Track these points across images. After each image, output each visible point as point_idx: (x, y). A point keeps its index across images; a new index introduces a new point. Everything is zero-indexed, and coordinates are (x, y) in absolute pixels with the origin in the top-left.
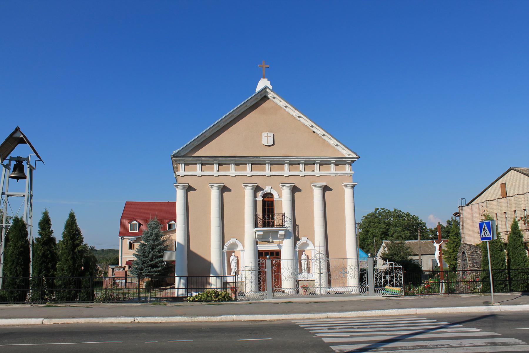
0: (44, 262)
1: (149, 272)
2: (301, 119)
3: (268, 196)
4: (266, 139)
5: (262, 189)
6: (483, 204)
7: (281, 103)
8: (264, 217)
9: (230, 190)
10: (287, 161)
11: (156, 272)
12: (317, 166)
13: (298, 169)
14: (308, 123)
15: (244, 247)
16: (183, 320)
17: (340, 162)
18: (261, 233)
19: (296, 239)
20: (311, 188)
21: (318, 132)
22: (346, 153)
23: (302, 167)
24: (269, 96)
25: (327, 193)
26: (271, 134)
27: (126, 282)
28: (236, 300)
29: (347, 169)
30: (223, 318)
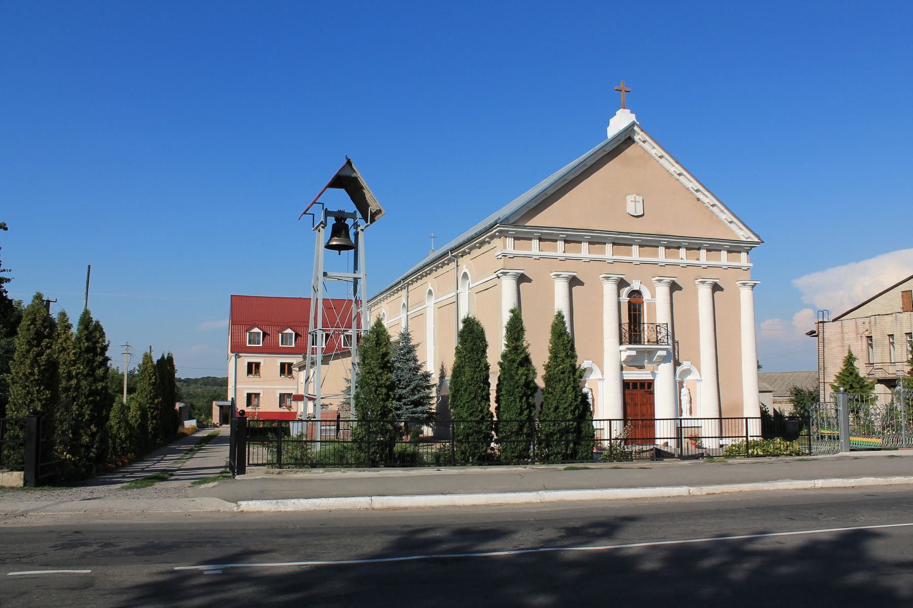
0: (525, 394)
1: (413, 413)
2: (681, 178)
3: (636, 294)
4: (633, 205)
5: (628, 285)
6: (864, 320)
7: (655, 150)
8: (630, 328)
9: (582, 284)
10: (665, 241)
11: (423, 413)
12: (703, 252)
13: (677, 256)
14: (693, 185)
15: (603, 374)
16: (878, 483)
17: (735, 248)
18: (634, 353)
19: (677, 364)
20: (695, 285)
21: (706, 200)
22: (743, 234)
23: (682, 252)
24: (636, 138)
25: (676, 294)
26: (639, 199)
27: (338, 429)
28: (810, 454)
29: (743, 259)
30: (819, 483)
